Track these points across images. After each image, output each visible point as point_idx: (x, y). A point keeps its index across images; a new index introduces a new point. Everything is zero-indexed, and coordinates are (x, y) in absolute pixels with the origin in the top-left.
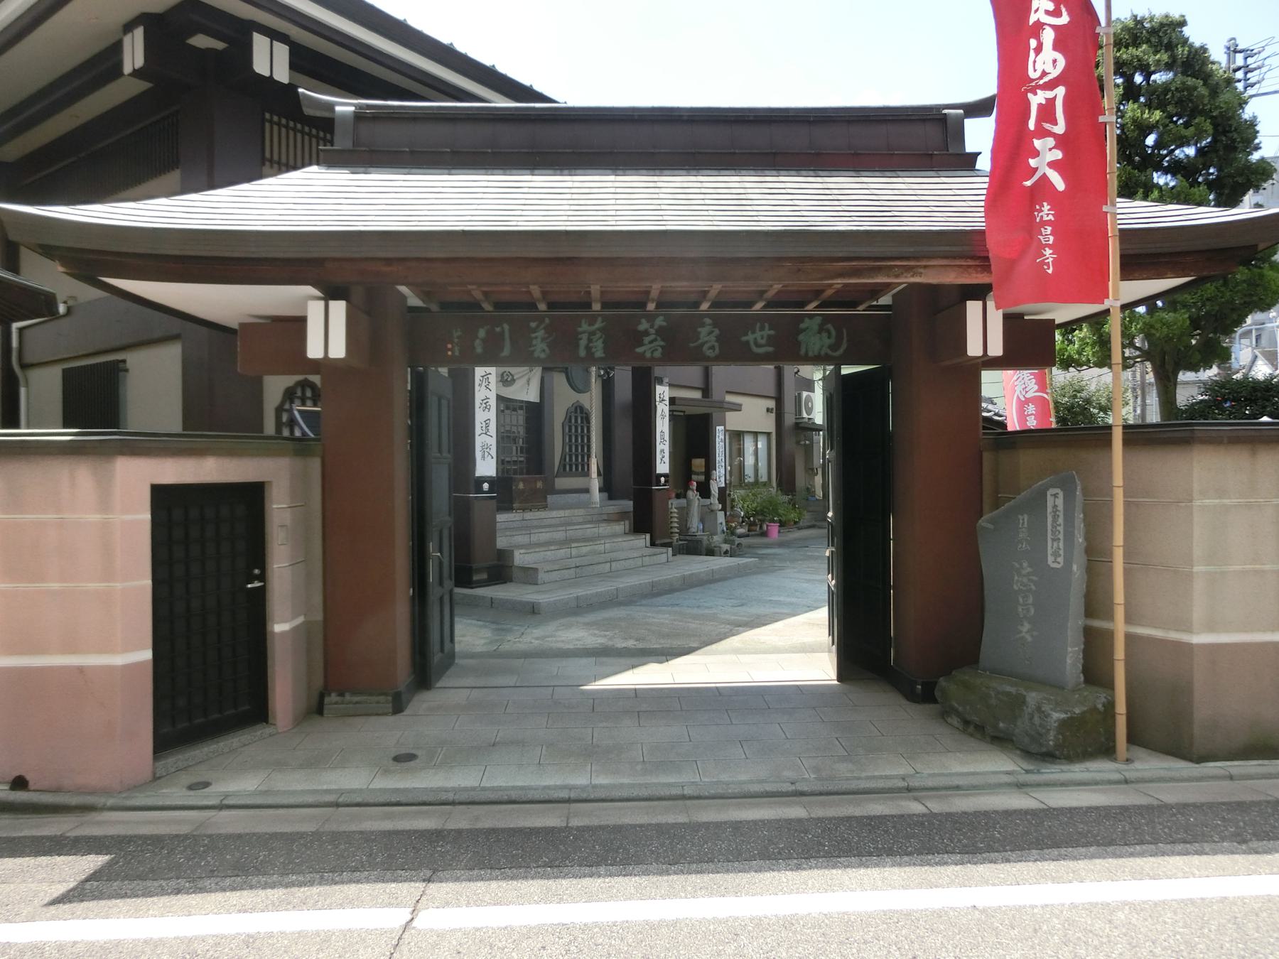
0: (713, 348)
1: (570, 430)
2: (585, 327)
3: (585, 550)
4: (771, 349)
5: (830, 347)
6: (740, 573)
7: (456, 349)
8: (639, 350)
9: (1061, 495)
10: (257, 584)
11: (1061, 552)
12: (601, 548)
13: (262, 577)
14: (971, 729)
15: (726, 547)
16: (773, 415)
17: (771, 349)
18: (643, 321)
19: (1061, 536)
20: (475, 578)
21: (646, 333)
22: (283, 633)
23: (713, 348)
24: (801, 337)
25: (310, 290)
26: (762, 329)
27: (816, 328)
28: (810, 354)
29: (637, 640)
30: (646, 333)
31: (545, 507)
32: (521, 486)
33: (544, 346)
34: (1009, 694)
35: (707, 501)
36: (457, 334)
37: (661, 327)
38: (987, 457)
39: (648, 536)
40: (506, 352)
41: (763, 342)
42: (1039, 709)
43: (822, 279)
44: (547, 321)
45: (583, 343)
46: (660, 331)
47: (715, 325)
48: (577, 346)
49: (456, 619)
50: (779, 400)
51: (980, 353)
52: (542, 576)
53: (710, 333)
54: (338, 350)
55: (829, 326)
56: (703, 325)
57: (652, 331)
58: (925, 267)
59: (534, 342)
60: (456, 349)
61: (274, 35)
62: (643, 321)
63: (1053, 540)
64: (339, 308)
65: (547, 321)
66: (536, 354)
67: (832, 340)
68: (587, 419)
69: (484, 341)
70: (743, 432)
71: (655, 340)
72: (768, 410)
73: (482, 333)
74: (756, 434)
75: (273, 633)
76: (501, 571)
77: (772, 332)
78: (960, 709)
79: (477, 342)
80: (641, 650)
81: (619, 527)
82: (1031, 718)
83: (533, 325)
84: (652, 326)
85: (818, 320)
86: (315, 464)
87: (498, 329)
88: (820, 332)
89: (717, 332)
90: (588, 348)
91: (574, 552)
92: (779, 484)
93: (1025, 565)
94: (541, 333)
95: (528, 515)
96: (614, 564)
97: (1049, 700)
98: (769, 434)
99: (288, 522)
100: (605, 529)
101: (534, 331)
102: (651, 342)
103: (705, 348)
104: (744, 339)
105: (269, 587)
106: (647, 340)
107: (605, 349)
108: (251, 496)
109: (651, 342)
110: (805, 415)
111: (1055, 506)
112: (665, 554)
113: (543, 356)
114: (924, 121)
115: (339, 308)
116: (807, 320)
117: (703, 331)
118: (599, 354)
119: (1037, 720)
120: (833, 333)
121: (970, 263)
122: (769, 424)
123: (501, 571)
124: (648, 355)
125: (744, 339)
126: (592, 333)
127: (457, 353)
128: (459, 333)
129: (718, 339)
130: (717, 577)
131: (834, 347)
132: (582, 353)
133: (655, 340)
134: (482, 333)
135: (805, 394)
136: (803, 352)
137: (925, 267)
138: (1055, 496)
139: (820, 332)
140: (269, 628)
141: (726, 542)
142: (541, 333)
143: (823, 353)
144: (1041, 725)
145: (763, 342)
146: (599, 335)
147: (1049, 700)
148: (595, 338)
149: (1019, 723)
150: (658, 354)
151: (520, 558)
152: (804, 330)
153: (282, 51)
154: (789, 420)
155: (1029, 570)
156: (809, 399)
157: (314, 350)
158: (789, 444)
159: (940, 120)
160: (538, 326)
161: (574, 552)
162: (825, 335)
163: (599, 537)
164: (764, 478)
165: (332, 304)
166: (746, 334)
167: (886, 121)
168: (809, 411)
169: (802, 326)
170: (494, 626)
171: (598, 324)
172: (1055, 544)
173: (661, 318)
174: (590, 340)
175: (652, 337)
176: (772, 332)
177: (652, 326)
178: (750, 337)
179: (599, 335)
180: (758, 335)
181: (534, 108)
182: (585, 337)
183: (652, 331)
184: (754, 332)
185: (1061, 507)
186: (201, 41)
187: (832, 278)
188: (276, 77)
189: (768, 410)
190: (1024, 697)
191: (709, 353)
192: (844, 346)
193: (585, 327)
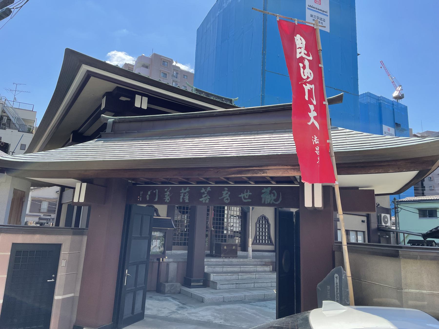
0: (227, 199)
2: (183, 191)
4: (250, 200)
5: (275, 200)
8: (201, 200)
10: (53, 280)
12: (254, 276)
13: (55, 278)
16: (365, 224)
17: (250, 200)
20: (192, 284)
21: (203, 193)
23: (227, 199)
24: (263, 196)
26: (247, 192)
27: (269, 192)
28: (266, 203)
30: (203, 193)
32: (225, 247)
37: (209, 191)
40: (156, 200)
41: (247, 197)
44: (170, 188)
45: (182, 197)
47: (228, 191)
48: (180, 198)
49: (147, 301)
52: (218, 286)
53: (227, 193)
55: (274, 191)
56: (224, 190)
57: (206, 192)
58: (268, 169)
59: (166, 196)
61: (142, 95)
62: (203, 189)
64: (84, 185)
65: (170, 188)
66: (166, 201)
67: (275, 197)
69: (149, 195)
71: (207, 196)
72: (363, 221)
73: (149, 193)
76: (206, 282)
77: (251, 194)
79: (148, 196)
81: (268, 268)
83: (166, 190)
85: (270, 189)
87: (154, 192)
88: (270, 194)
89: (229, 193)
90: (183, 199)
94: (168, 193)
96: (256, 285)
101: (166, 192)
102: (205, 197)
103: (225, 199)
104: (240, 196)
106: (204, 196)
107: (189, 199)
108: (58, 247)
109: (205, 197)
110: (383, 224)
113: (168, 201)
115: (84, 185)
116: (265, 189)
121: (289, 167)
123: (206, 282)
124: (204, 202)
125: (240, 196)
126: (185, 193)
131: (276, 200)
132: (181, 201)
133: (207, 196)
134: (149, 193)
135: (383, 215)
136: (263, 202)
137: (268, 169)
139: (270, 194)
143: (271, 202)
145: (247, 197)
146: (187, 194)
148: (186, 195)
151: (213, 277)
153: (145, 99)
154: (374, 225)
156: (385, 217)
161: (240, 277)
162: (272, 195)
163: (257, 272)
166: (241, 194)
168: (386, 222)
169: (263, 191)
174: (184, 196)
175: (206, 195)
176: (251, 194)
177: (206, 191)
178: (242, 195)
180: (245, 194)
181: (126, 118)
182: (182, 194)
184: (243, 193)
186: (123, 99)
187: (230, 174)
188: (142, 107)
192: (280, 200)
193: (183, 191)
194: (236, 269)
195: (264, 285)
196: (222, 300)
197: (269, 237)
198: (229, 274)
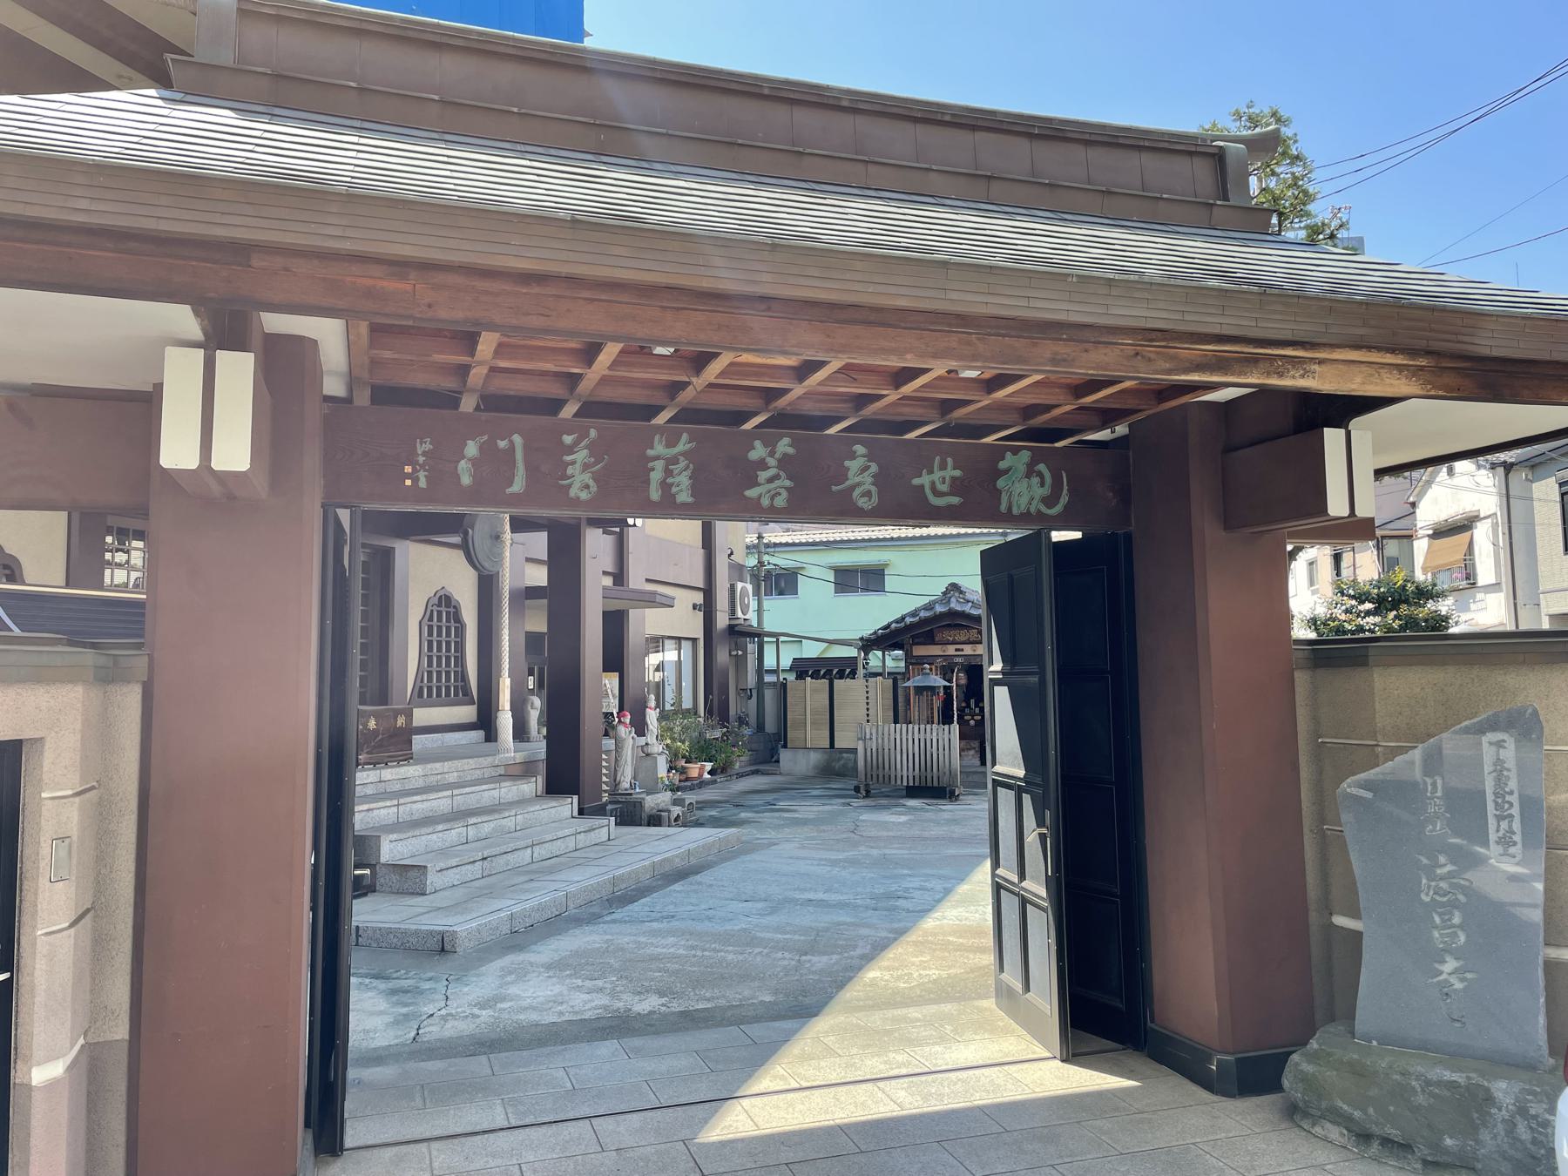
1: (430, 634)
2: (659, 448)
3: (487, 828)
4: (955, 500)
6: (726, 854)
7: (422, 475)
8: (751, 493)
9: (1510, 743)
11: (1517, 838)
12: (509, 823)
14: (1375, 1147)
15: (677, 810)
17: (955, 500)
18: (757, 443)
19: (1515, 811)
22: (52, 1085)
23: (868, 494)
24: (1001, 483)
25: (182, 319)
26: (943, 467)
27: (1022, 468)
28: (1015, 511)
29: (661, 994)
31: (408, 758)
33: (587, 478)
34: (1452, 1085)
35: (642, 741)
36: (423, 447)
37: (785, 455)
38: (1302, 679)
39: (576, 798)
41: (944, 488)
42: (1522, 1111)
43: (1169, 372)
45: (656, 476)
46: (784, 462)
48: (647, 482)
50: (709, 592)
51: (1346, 513)
53: (865, 469)
54: (234, 452)
55: (1042, 467)
56: (853, 456)
58: (1321, 362)
59: (570, 471)
60: (422, 475)
63: (1499, 818)
66: (573, 492)
67: (1046, 491)
68: (456, 616)
69: (475, 462)
70: (663, 638)
73: (471, 449)
74: (679, 639)
75: (29, 1087)
77: (957, 473)
78: (1357, 1114)
79: (463, 464)
80: (685, 1014)
82: (1511, 1126)
83: (568, 439)
84: (772, 454)
86: (130, 700)
87: (502, 444)
88: (1028, 475)
89: (874, 468)
90: (665, 486)
91: (472, 832)
92: (709, 711)
93: (1442, 859)
94: (581, 456)
95: (388, 774)
96: (537, 849)
97: (1534, 1093)
98: (694, 640)
99: (73, 829)
100: (510, 791)
101: (571, 450)
102: (770, 480)
104: (916, 481)
105: (24, 980)
106: (763, 476)
107: (695, 490)
110: (739, 614)
111: (1499, 762)
112: (605, 827)
113: (584, 495)
114: (1190, 154)
117: (853, 465)
118: (684, 497)
119: (1523, 1132)
120: (1048, 476)
122: (694, 626)
124: (765, 502)
125: (916, 481)
126: (673, 460)
127: (423, 483)
128: (427, 446)
129: (878, 480)
130: (693, 861)
131: (1050, 501)
132: (655, 495)
134: (471, 449)
136: (1003, 508)
137: (1321, 362)
138: (1500, 744)
139: (1028, 475)
140: (17, 1076)
141: (676, 802)
142: (581, 456)
144: (1534, 1142)
145: (944, 488)
146: (683, 463)
147: (1534, 1093)
148: (676, 468)
149: (1485, 1136)
150: (780, 502)
151: (390, 850)
152: (1006, 471)
154: (722, 621)
155: (1450, 868)
157: (177, 451)
158: (722, 656)
159: (1213, 155)
160: (576, 443)
161: (472, 832)
162: (1035, 480)
164: (687, 704)
165: (222, 357)
167: (1140, 148)
169: (1002, 465)
170: (382, 985)
171: (683, 446)
172: (1504, 825)
173: (786, 440)
174: (668, 472)
176: (957, 473)
177: (772, 454)
178: (924, 480)
179: (683, 463)
182: (659, 465)
183: (771, 462)
185: (1511, 763)
187: (1187, 371)
189: (695, 607)
190: (1488, 1090)
191: (863, 503)
192: (1064, 499)
193: (659, 448)
194: (440, 803)
195: (558, 847)
196: (505, 929)
197: (463, 677)
198: (440, 827)
